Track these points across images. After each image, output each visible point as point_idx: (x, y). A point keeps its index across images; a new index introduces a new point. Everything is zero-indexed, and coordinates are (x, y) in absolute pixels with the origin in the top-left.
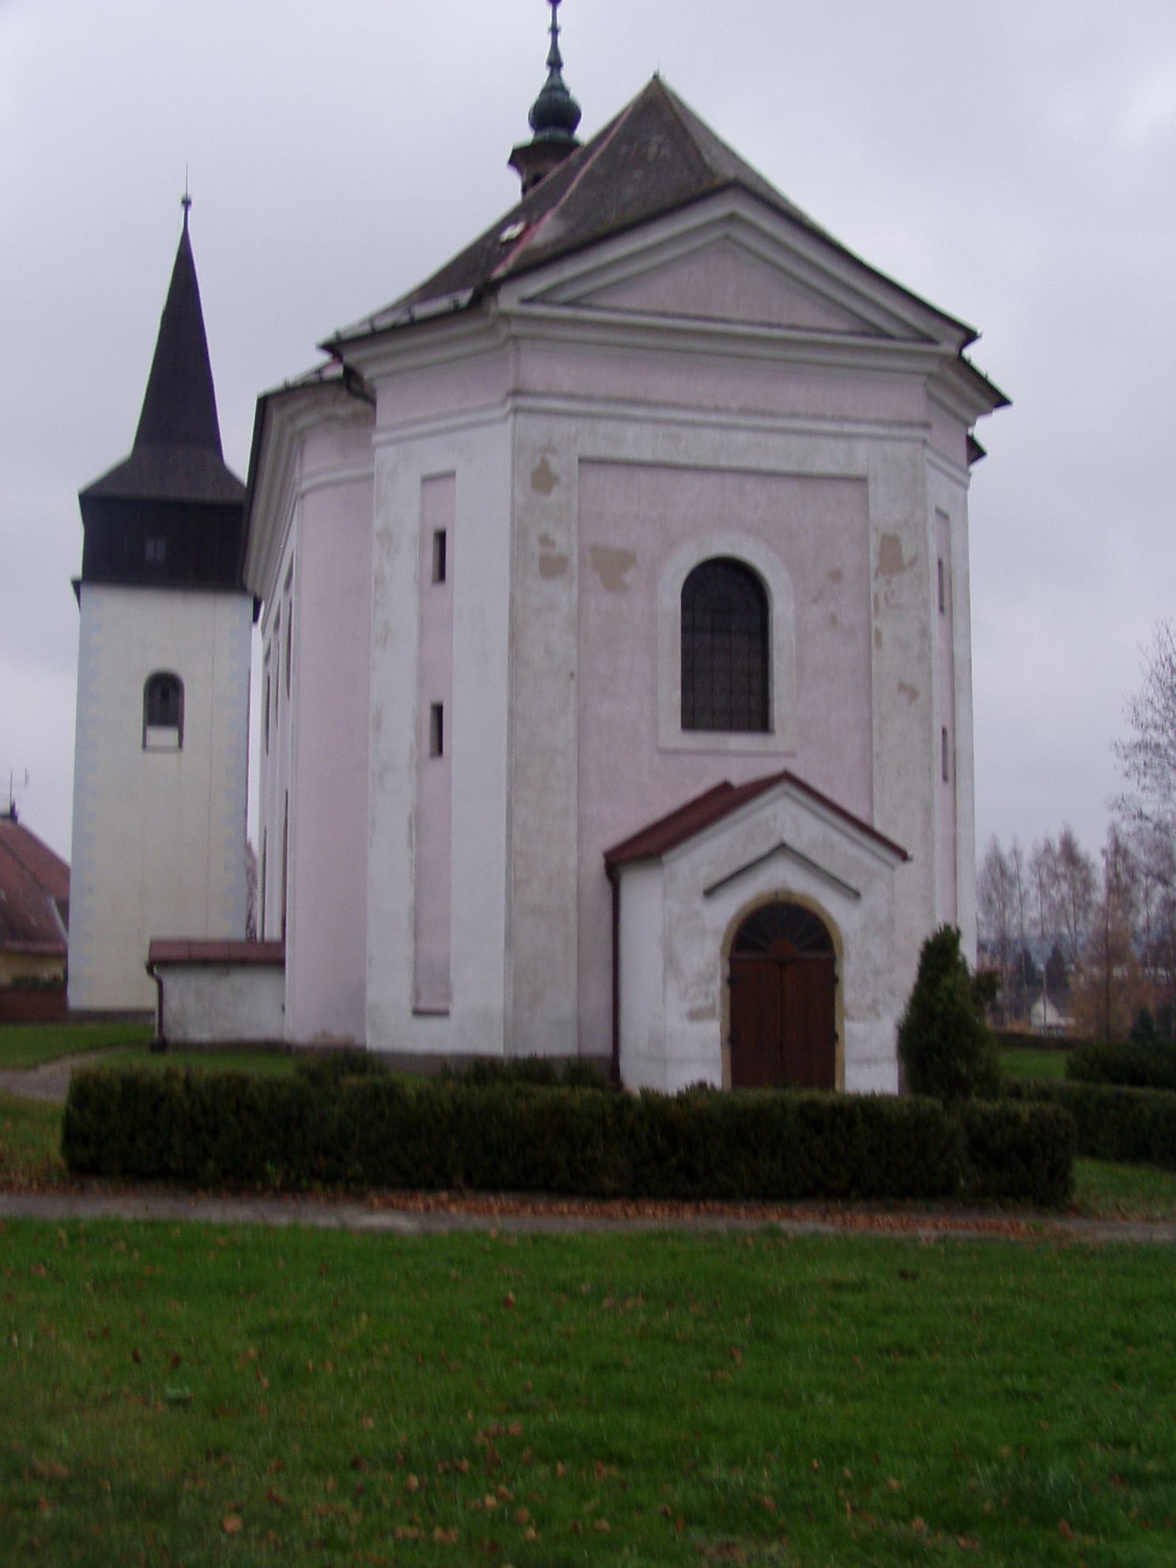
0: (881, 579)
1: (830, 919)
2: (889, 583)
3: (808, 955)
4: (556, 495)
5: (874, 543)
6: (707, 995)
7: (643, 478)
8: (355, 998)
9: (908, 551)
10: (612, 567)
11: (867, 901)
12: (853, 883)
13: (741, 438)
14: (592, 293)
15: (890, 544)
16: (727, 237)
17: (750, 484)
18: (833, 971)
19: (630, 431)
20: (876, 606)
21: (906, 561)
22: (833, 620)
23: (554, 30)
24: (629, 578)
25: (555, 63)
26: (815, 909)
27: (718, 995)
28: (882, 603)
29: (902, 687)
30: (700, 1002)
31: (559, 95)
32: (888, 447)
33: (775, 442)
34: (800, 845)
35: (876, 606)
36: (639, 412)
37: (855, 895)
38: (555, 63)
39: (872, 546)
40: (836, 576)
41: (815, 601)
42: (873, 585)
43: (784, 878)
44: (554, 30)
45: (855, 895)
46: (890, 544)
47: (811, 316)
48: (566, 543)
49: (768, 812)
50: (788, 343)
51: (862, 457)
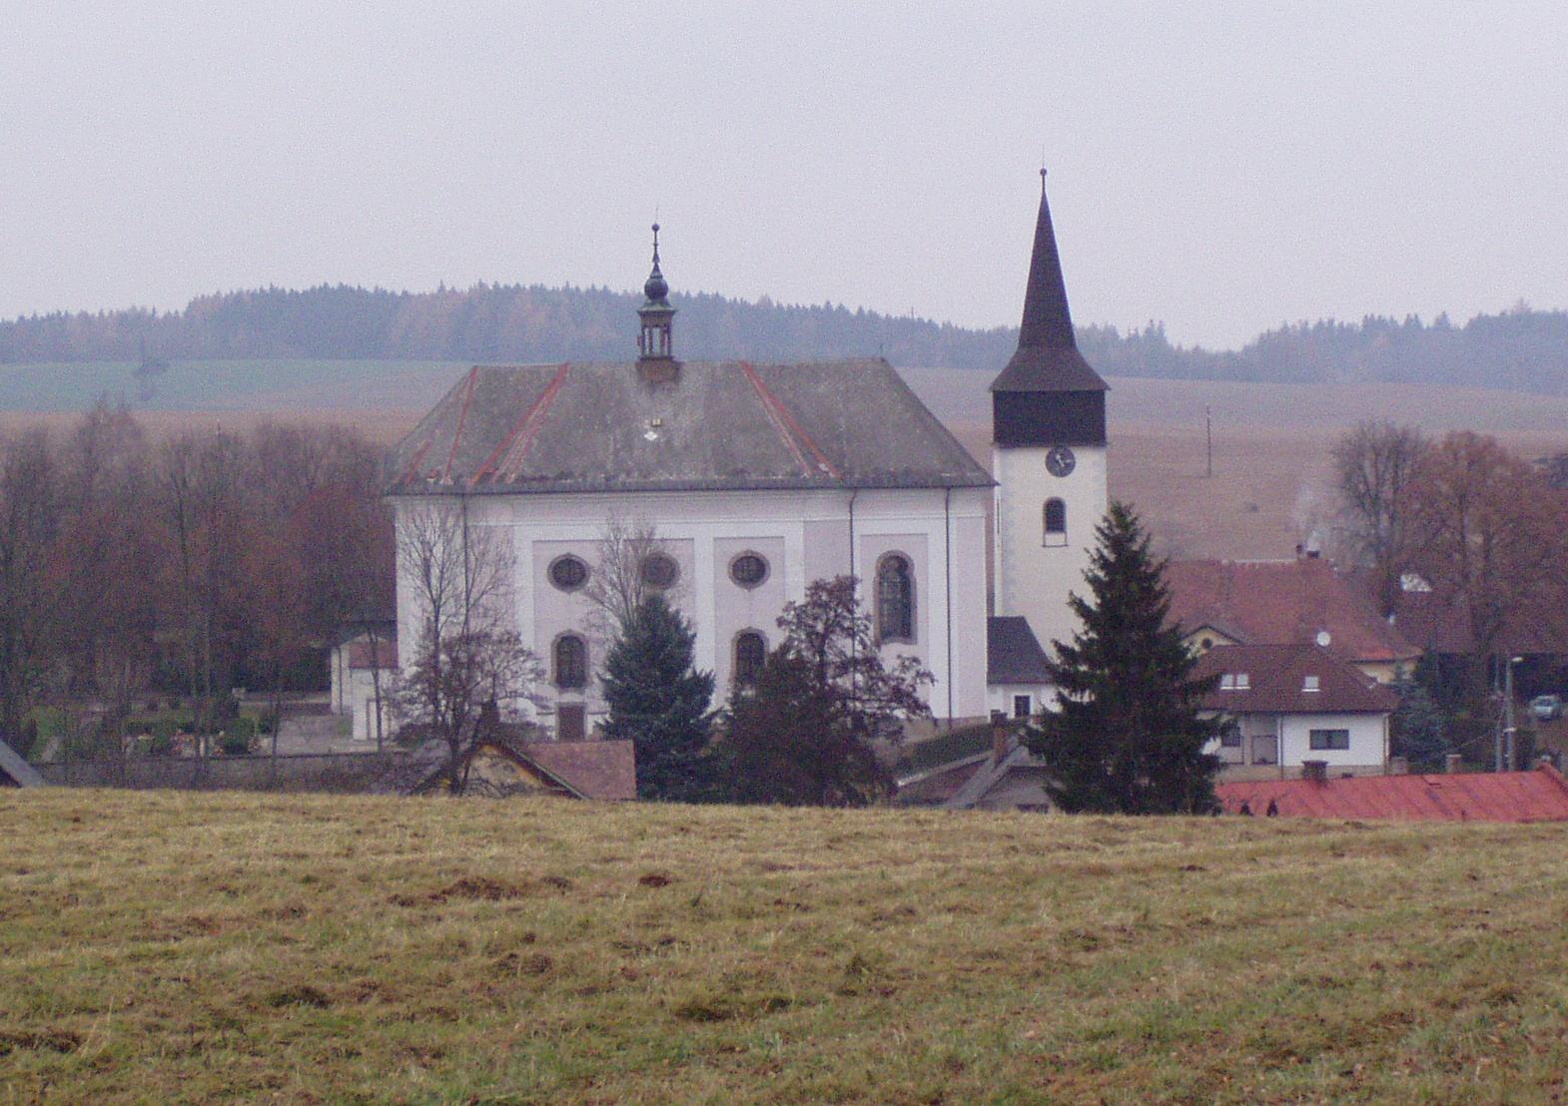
25: (656, 258)
38: (656, 258)
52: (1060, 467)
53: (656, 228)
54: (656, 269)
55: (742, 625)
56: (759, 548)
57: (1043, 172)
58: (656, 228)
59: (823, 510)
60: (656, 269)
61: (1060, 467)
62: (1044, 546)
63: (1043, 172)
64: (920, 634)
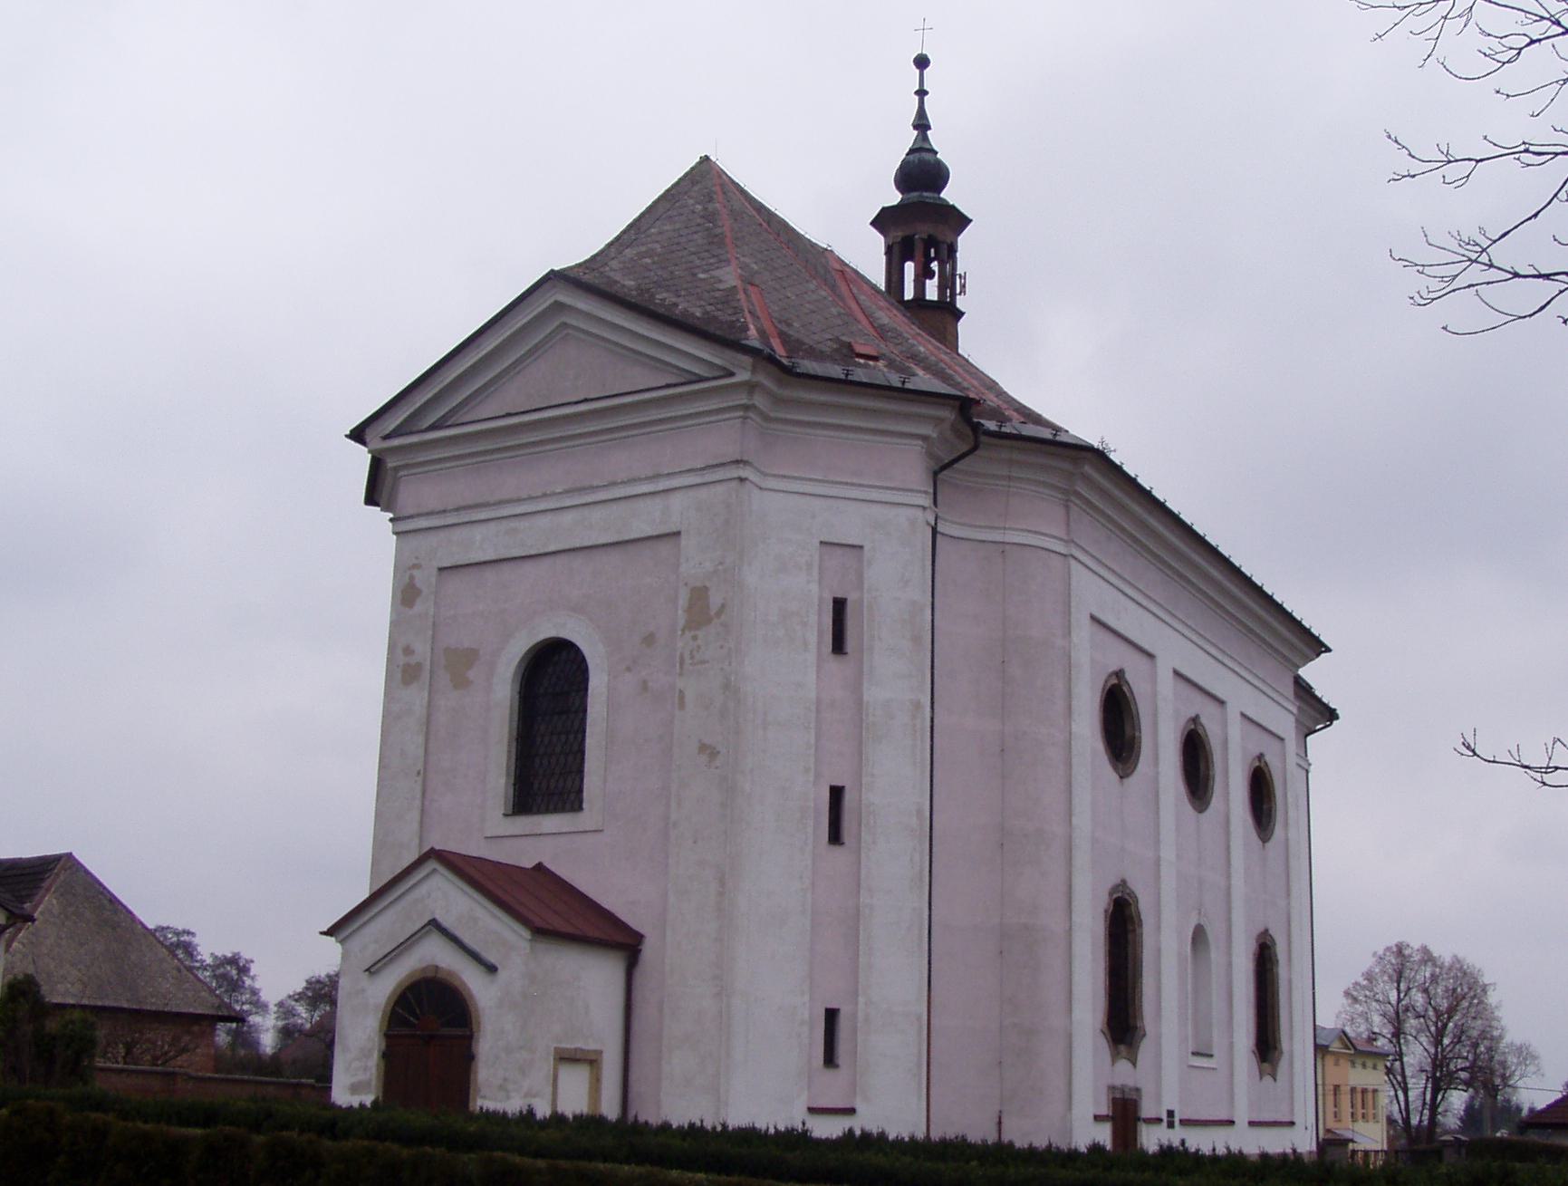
0: (688, 634)
1: (471, 996)
2: (695, 638)
3: (446, 1031)
4: (419, 607)
5: (683, 599)
6: (366, 1069)
7: (490, 574)
8: (484, 1097)
9: (715, 600)
10: (462, 664)
11: (503, 974)
12: (491, 957)
13: (568, 518)
14: (453, 411)
15: (699, 595)
16: (565, 325)
17: (578, 561)
18: (469, 1047)
19: (478, 533)
20: (682, 664)
21: (713, 610)
22: (644, 686)
23: (922, 93)
24: (471, 674)
25: (922, 124)
26: (457, 983)
27: (374, 1070)
28: (688, 661)
29: (703, 748)
30: (361, 1077)
31: (927, 156)
32: (703, 493)
33: (597, 514)
34: (446, 922)
35: (682, 664)
36: (483, 515)
37: (492, 969)
38: (922, 124)
39: (681, 602)
40: (649, 640)
41: (629, 669)
42: (680, 644)
43: (435, 954)
44: (922, 93)
45: (492, 969)
46: (699, 595)
47: (640, 377)
48: (422, 650)
49: (423, 890)
50: (567, 419)
51: (676, 511)
53: (922, 62)
58: (922, 62)
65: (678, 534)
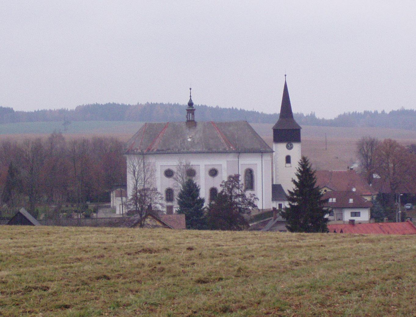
25: (191, 96)
38: (191, 96)
52: (290, 148)
53: (190, 89)
54: (191, 99)
55: (211, 186)
56: (216, 167)
57: (285, 75)
58: (190, 89)
59: (231, 158)
60: (191, 99)
61: (290, 148)
62: (286, 167)
63: (285, 75)
64: (255, 189)
65: (199, 165)
